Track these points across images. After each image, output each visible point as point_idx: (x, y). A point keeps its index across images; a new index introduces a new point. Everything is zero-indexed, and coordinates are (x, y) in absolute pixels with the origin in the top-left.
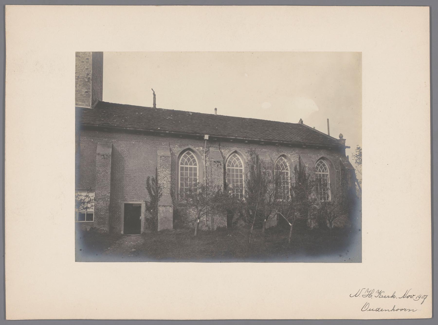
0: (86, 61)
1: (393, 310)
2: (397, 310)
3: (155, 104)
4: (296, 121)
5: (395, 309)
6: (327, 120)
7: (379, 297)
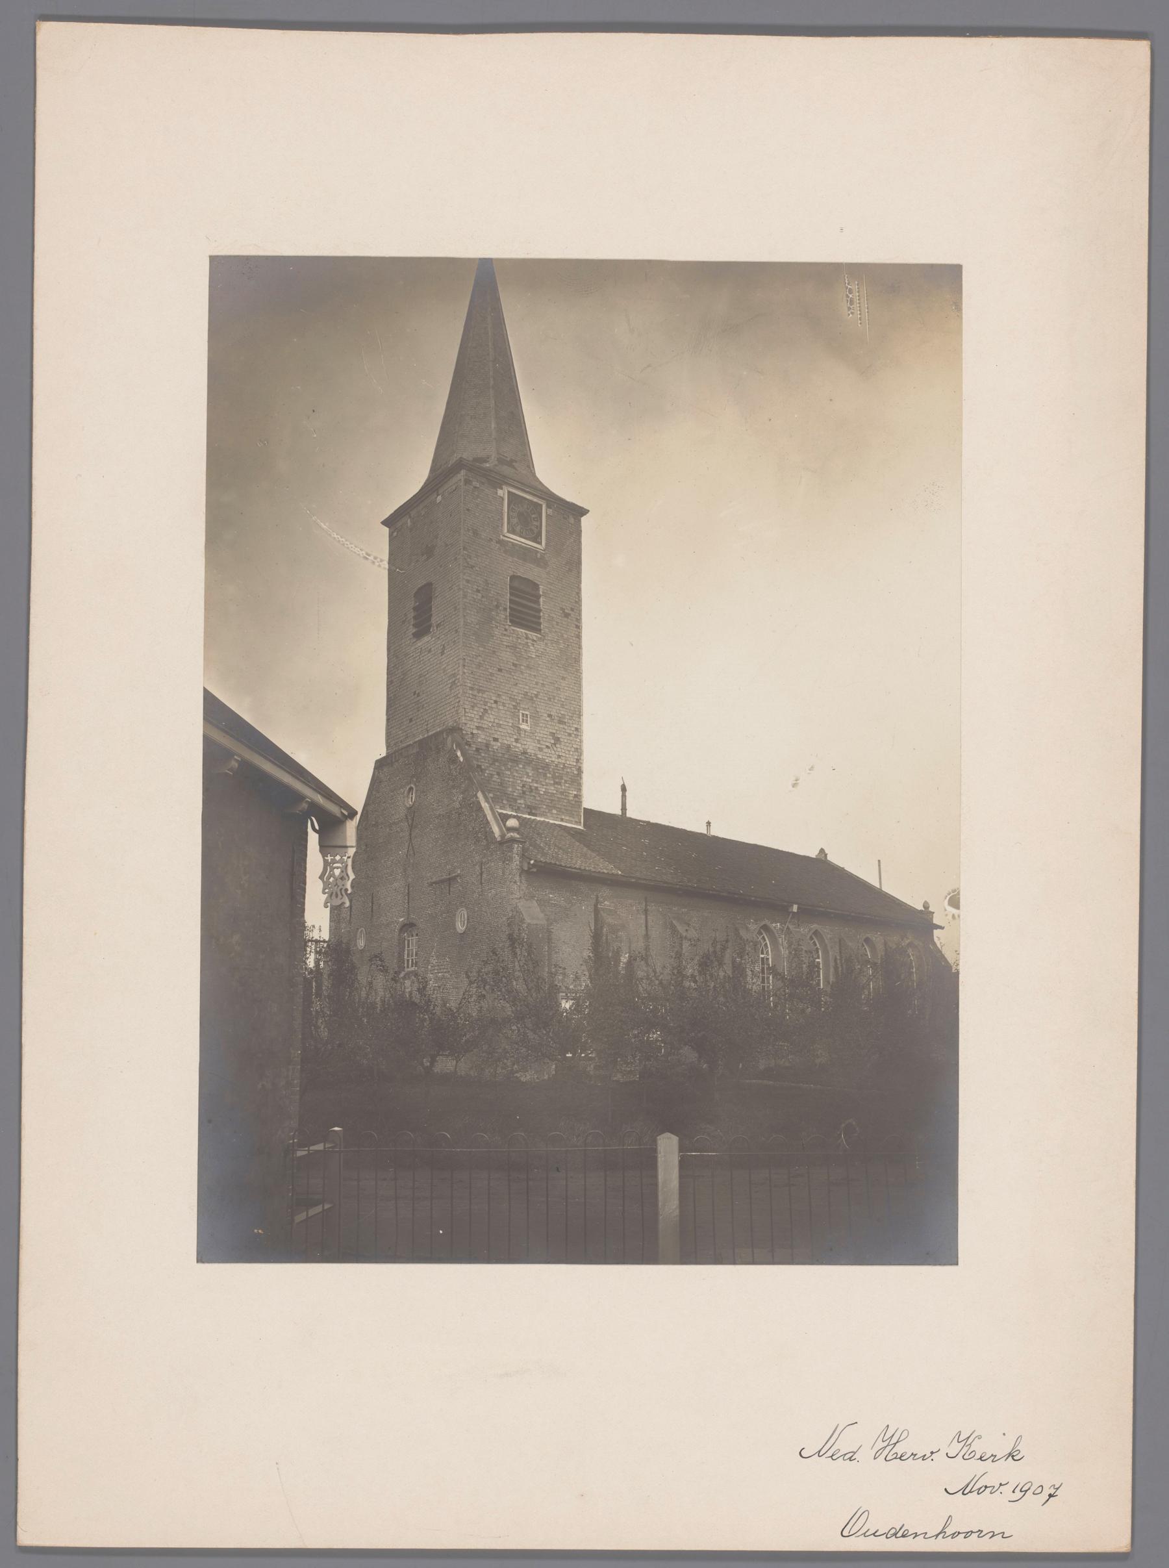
0: (575, 733)
1: (941, 1535)
2: (953, 1536)
3: (624, 809)
4: (813, 853)
5: (949, 1531)
6: (877, 862)
7: (958, 1442)
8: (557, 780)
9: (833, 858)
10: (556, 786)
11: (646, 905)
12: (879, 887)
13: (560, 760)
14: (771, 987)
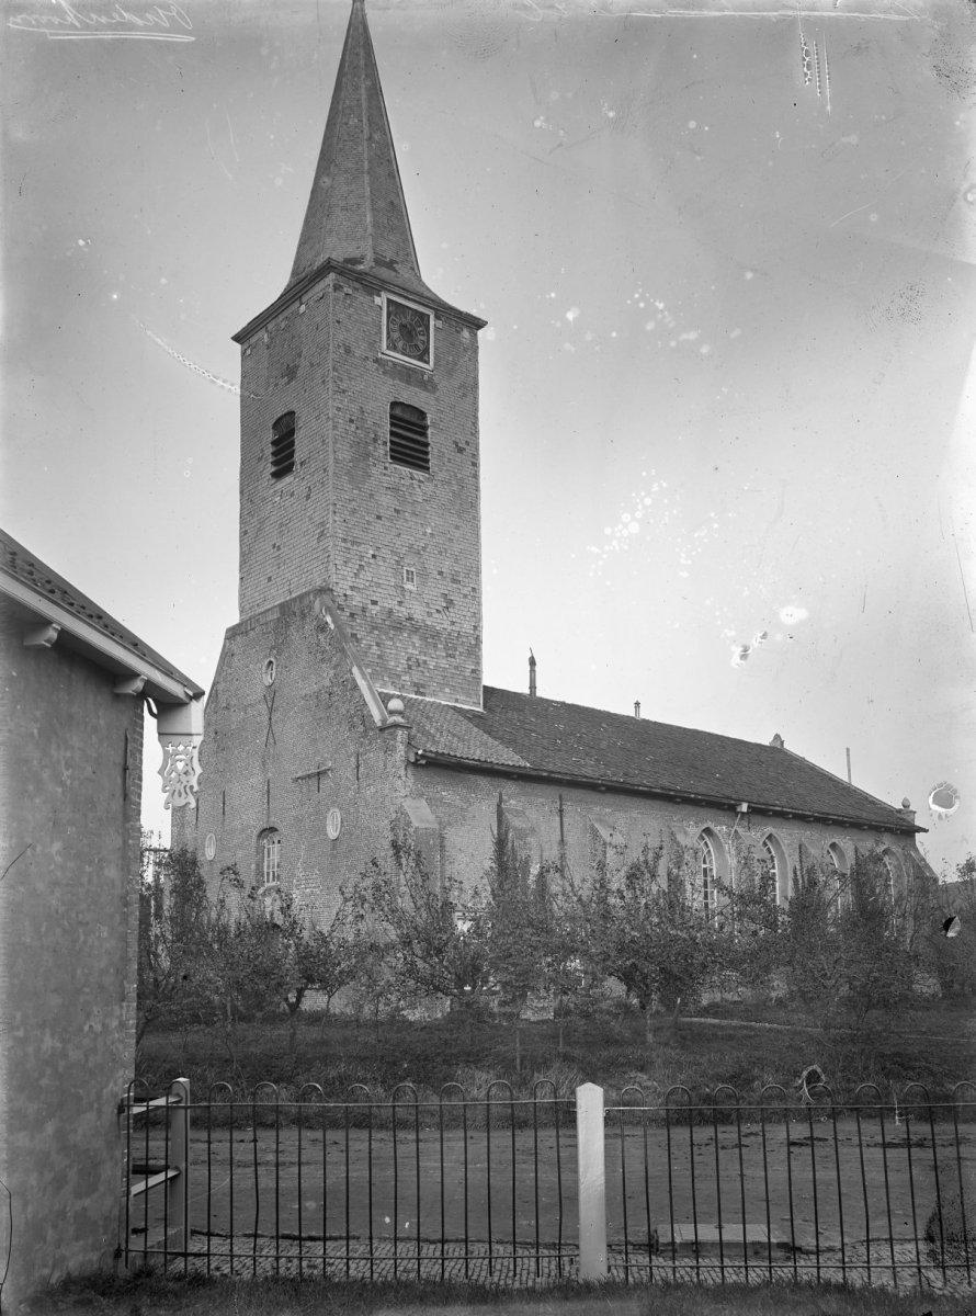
3: (533, 687)
4: (766, 740)
9: (791, 746)
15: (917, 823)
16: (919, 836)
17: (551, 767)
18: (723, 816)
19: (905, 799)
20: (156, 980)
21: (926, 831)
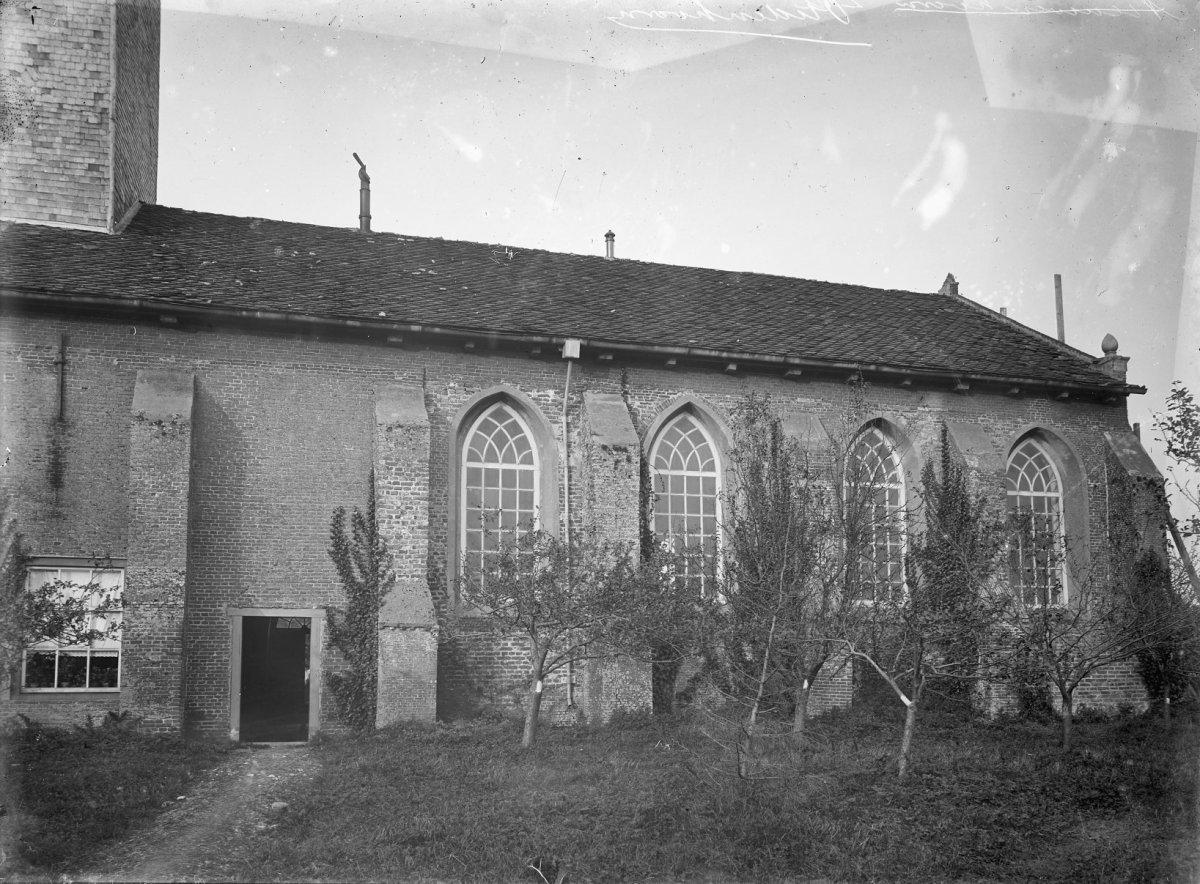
3: (365, 216)
4: (933, 286)
8: (43, 139)
9: (972, 291)
10: (38, 150)
11: (62, 352)
12: (1055, 336)
13: (48, 98)
14: (774, 620)
15: (1130, 380)
16: (1132, 400)
17: (829, 352)
18: (541, 370)
19: (1109, 338)
20: (751, 867)
21: (1142, 390)
